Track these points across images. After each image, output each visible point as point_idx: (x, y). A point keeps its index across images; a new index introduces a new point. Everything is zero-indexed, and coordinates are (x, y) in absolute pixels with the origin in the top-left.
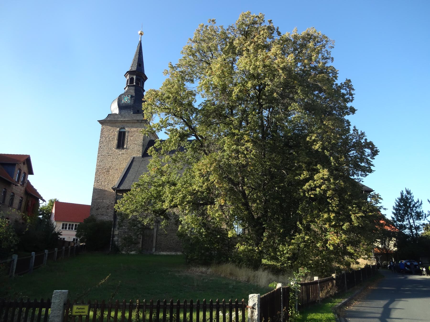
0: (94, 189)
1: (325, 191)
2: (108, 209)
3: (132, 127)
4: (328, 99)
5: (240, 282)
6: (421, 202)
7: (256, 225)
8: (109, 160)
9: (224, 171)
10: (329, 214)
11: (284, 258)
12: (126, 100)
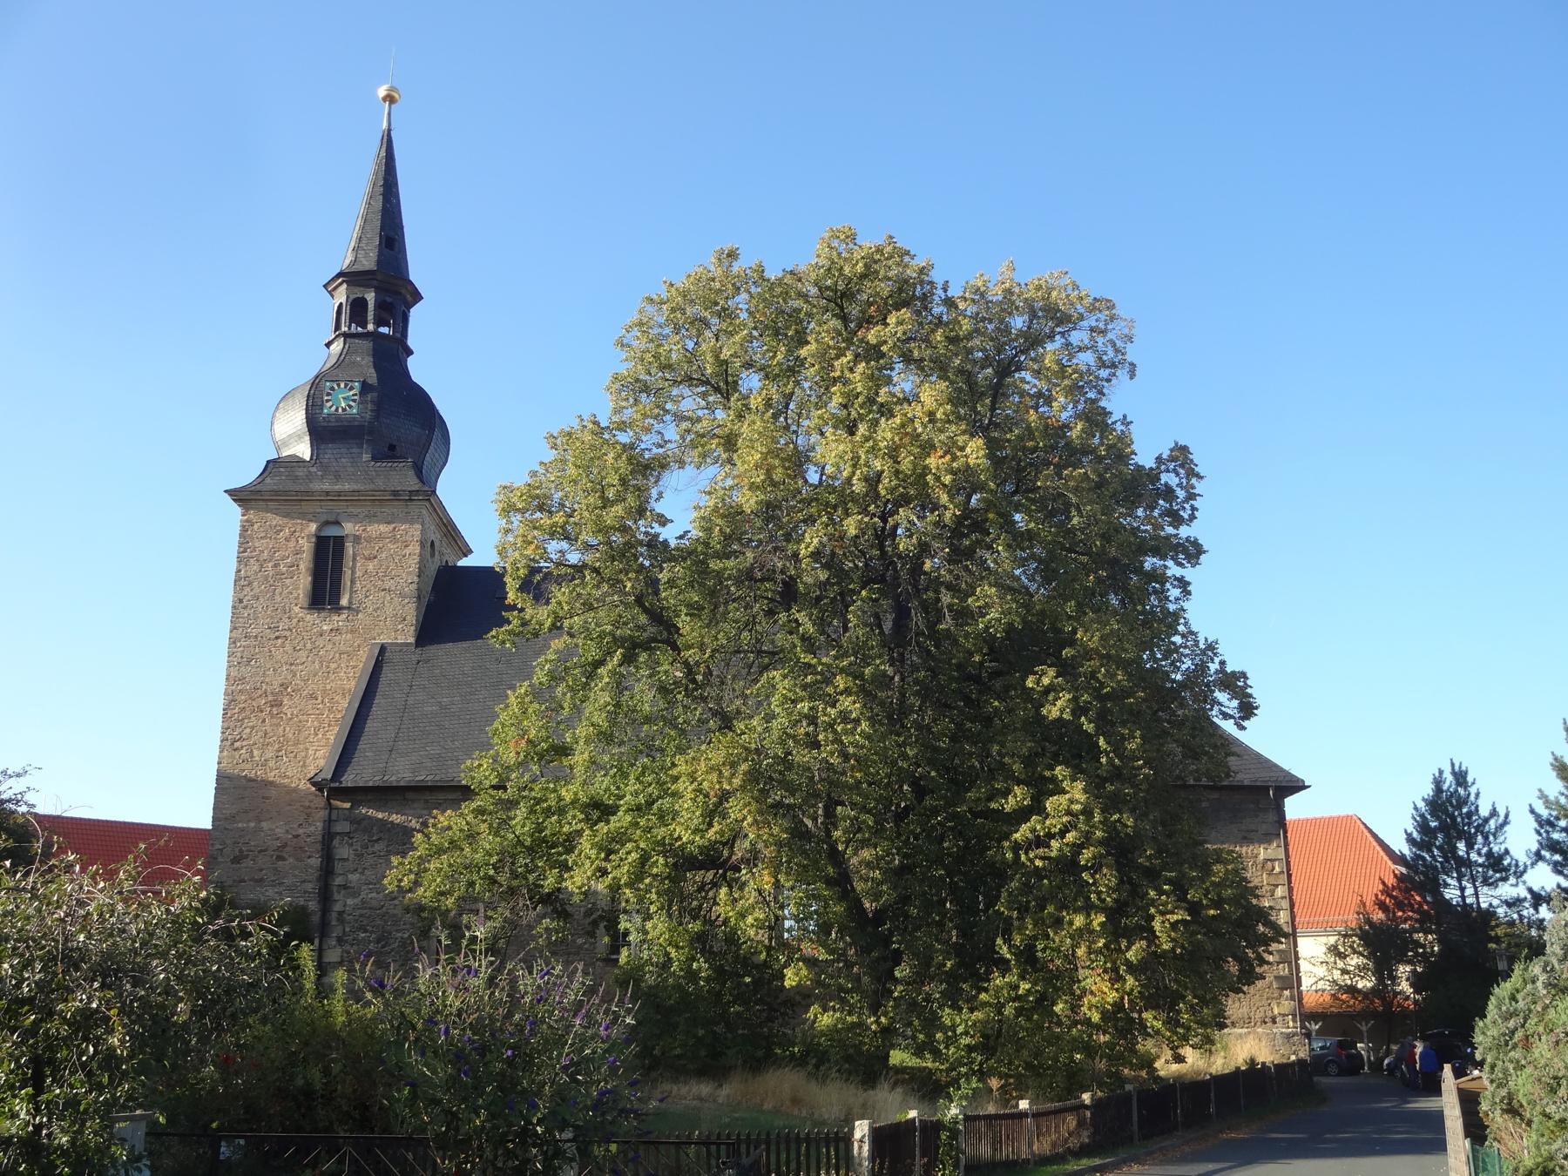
0: (222, 778)
1: (1077, 848)
2: (280, 858)
3: (371, 518)
4: (1104, 529)
5: (824, 1123)
6: (1507, 816)
7: (870, 937)
8: (278, 654)
9: (768, 779)
10: (1088, 915)
11: (958, 1048)
12: (343, 402)
